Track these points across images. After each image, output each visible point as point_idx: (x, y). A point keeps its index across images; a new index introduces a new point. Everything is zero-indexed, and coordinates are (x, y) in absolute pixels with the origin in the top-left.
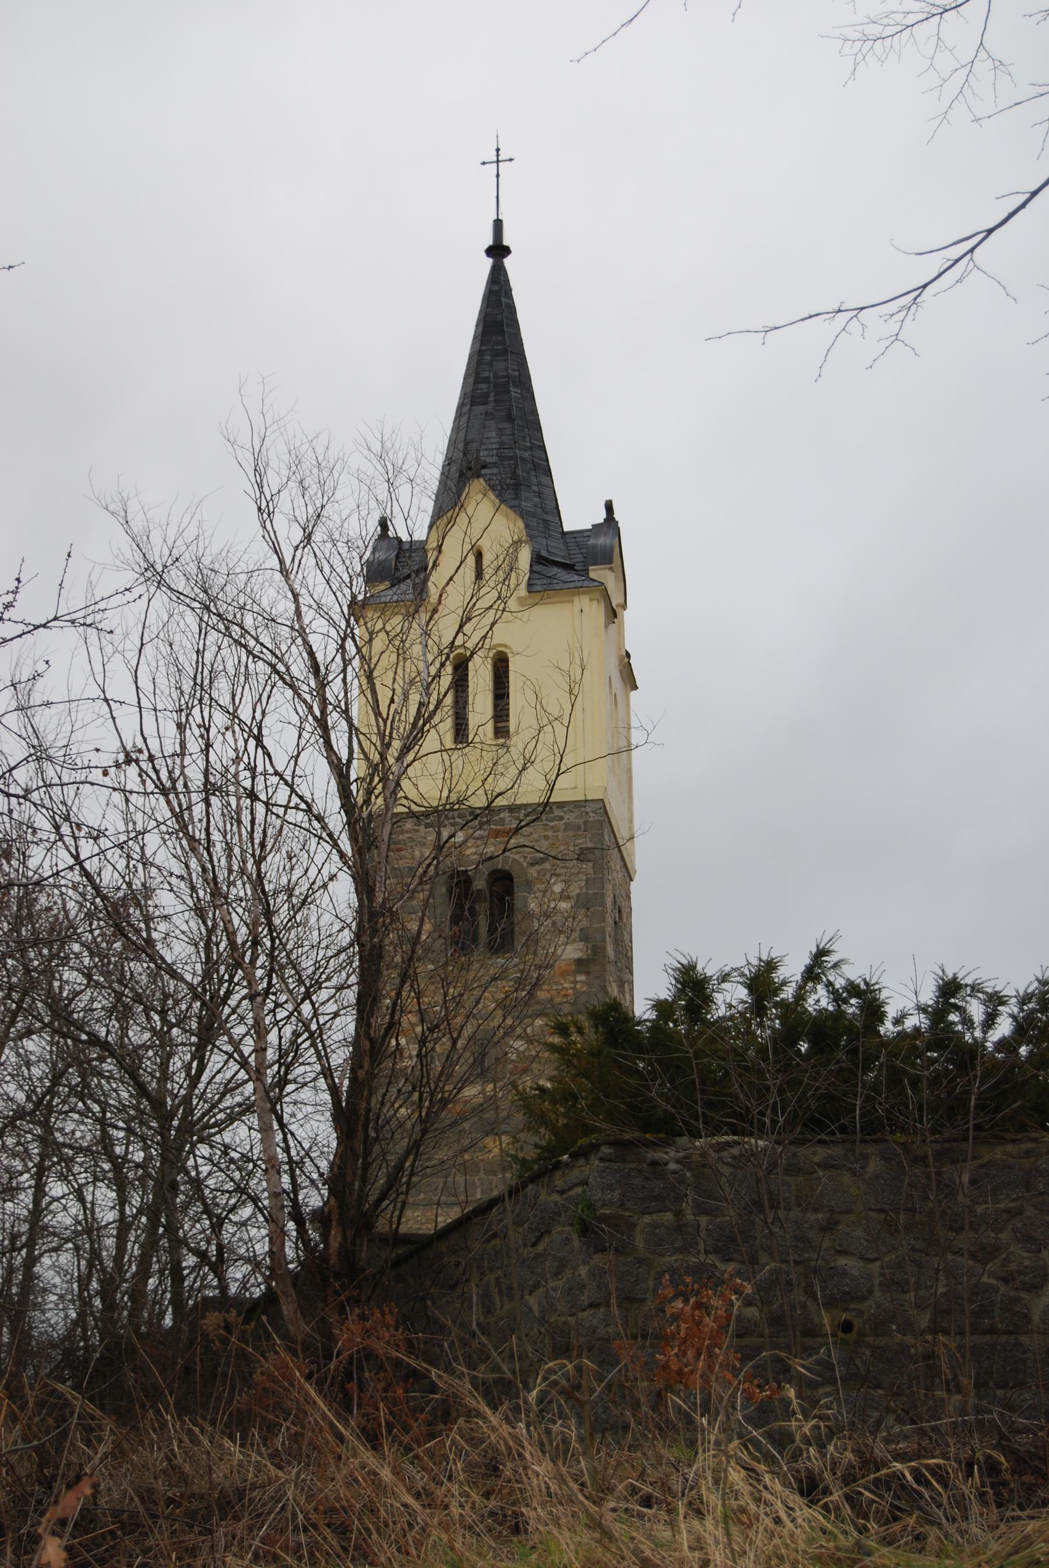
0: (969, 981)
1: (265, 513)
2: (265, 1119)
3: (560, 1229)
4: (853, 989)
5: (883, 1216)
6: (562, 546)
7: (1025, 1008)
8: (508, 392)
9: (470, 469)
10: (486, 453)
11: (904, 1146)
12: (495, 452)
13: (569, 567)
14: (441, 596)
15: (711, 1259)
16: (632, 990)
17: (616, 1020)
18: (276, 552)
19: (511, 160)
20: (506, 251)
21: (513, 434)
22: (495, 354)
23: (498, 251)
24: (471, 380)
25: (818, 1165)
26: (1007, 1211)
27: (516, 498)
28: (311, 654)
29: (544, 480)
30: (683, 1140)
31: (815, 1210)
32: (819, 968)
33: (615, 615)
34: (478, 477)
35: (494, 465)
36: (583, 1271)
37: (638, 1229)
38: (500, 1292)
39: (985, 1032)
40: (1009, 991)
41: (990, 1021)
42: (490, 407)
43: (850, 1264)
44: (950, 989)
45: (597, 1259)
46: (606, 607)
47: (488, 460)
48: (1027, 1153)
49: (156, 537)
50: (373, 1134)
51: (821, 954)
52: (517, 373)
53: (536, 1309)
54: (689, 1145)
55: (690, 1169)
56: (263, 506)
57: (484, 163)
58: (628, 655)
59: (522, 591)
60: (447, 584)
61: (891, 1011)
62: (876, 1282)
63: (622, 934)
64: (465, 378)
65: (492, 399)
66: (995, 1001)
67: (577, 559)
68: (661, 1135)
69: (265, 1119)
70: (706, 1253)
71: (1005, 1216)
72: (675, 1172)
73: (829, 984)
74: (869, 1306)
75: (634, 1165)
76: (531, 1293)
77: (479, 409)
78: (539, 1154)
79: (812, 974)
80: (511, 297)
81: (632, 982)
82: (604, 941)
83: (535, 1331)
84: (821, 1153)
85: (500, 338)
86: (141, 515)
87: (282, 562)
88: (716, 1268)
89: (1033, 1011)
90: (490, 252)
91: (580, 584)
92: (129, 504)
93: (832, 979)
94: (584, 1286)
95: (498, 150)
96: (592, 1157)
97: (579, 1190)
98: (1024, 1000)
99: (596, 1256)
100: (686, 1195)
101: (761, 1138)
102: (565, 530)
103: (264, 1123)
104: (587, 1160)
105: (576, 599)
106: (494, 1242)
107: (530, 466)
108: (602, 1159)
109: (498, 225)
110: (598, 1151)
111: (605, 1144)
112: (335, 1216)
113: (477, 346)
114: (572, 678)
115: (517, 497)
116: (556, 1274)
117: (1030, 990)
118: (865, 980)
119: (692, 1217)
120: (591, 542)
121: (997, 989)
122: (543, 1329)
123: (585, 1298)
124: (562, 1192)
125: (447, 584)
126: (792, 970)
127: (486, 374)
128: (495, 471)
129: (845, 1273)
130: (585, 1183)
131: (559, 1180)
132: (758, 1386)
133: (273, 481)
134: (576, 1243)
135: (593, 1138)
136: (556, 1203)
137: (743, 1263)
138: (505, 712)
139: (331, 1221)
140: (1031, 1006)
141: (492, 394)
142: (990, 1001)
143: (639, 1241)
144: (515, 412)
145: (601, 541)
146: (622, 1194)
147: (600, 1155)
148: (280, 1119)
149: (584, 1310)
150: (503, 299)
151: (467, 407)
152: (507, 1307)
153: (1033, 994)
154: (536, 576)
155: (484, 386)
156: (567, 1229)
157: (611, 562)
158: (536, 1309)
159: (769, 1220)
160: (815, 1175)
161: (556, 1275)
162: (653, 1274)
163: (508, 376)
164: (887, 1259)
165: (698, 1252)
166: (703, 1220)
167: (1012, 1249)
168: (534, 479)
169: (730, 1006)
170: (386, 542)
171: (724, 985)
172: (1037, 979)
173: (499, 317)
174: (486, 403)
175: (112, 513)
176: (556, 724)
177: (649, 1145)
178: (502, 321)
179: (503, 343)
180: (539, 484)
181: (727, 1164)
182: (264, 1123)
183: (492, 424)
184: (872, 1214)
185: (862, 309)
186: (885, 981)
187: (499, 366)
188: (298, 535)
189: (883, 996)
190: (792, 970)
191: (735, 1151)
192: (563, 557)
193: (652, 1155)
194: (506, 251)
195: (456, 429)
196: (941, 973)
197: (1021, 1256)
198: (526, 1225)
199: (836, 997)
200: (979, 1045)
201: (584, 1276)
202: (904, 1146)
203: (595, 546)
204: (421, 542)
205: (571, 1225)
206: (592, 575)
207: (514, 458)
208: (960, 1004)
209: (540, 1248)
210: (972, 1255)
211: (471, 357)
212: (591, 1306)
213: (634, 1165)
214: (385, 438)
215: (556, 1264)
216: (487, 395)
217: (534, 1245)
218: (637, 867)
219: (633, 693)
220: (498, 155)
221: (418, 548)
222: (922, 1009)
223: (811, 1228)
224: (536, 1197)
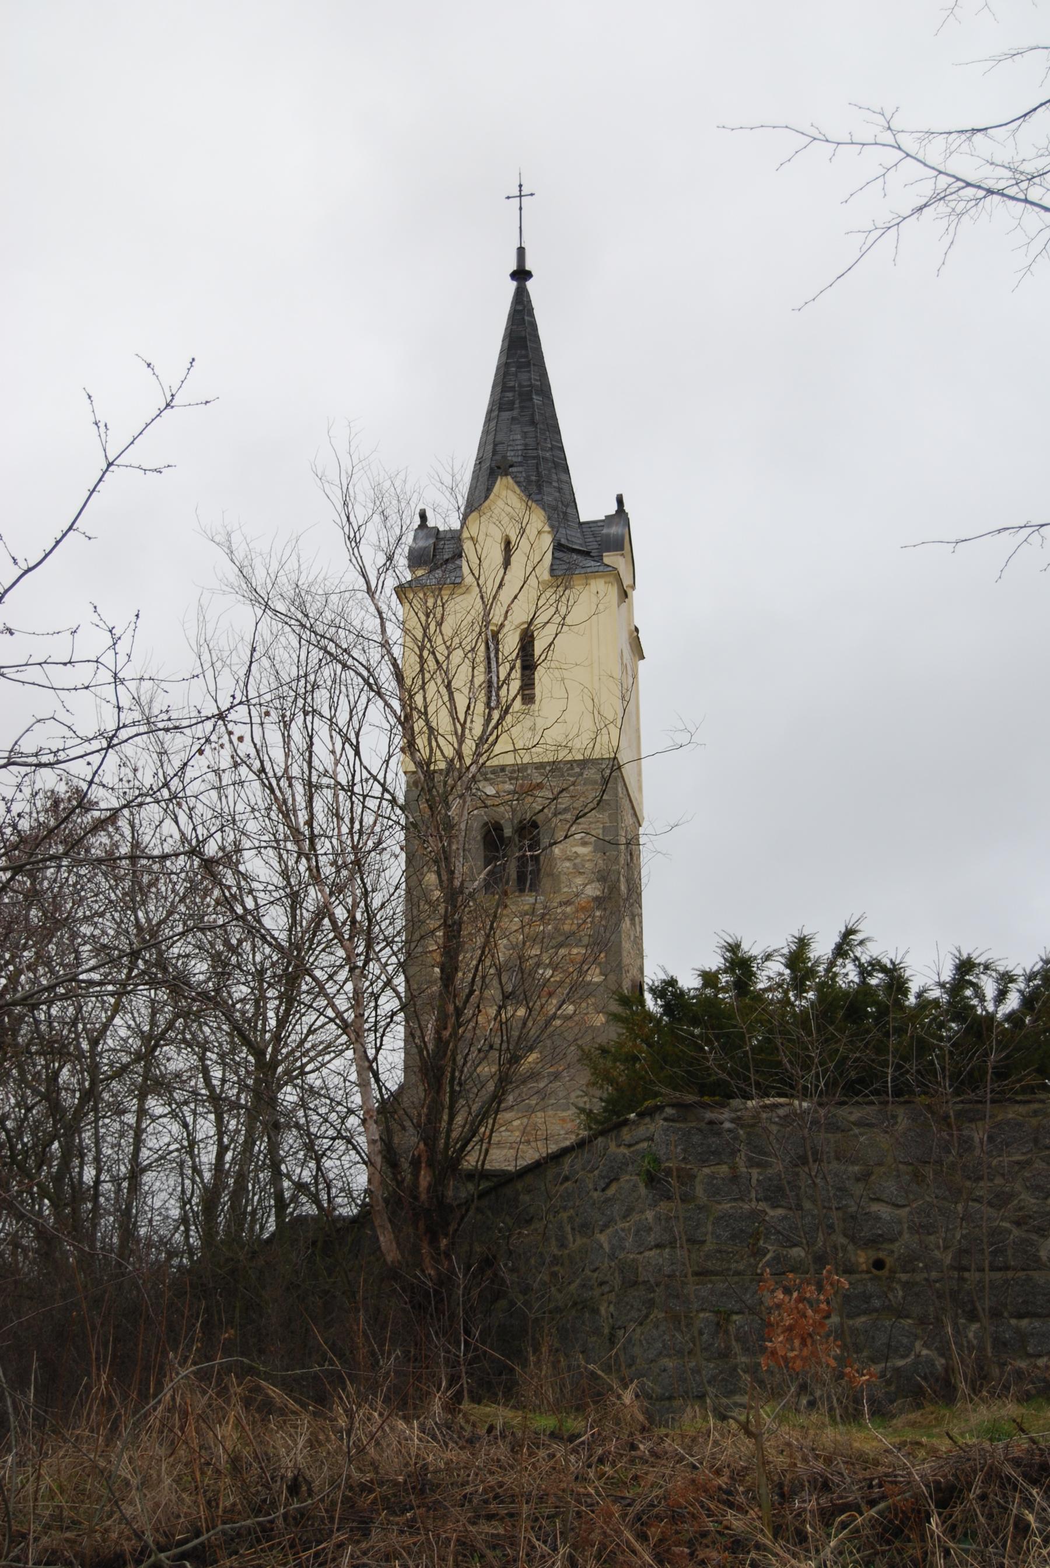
0: (981, 960)
1: (354, 541)
2: (364, 1076)
3: (627, 1178)
4: (877, 965)
5: (910, 1168)
6: (579, 535)
7: (1031, 984)
8: (531, 399)
9: (499, 468)
10: (512, 453)
11: (929, 1107)
12: (520, 453)
13: (587, 554)
14: (507, 612)
15: (762, 1206)
16: (641, 922)
17: (673, 994)
18: (364, 576)
19: (532, 195)
20: (528, 275)
21: (536, 437)
22: (520, 366)
23: (521, 275)
24: (499, 389)
25: (854, 1124)
26: (1018, 1163)
27: (540, 493)
28: (395, 664)
29: (563, 477)
30: (736, 1102)
31: (853, 1163)
32: (848, 945)
33: (626, 596)
34: (506, 475)
35: (520, 464)
36: (650, 1215)
37: (698, 1180)
38: (573, 1229)
39: (997, 1006)
40: (1018, 971)
41: (1001, 996)
42: (515, 413)
43: (884, 1211)
44: (965, 966)
45: (663, 1206)
46: (618, 588)
47: (515, 459)
48: (1035, 1113)
49: (258, 563)
50: (458, 1089)
51: (849, 932)
52: (538, 383)
53: (606, 1246)
54: (742, 1107)
55: (742, 1126)
56: (352, 536)
57: (508, 198)
58: (637, 630)
59: (546, 576)
60: (513, 602)
61: (914, 987)
62: (905, 1226)
63: (633, 874)
64: (493, 387)
65: (517, 406)
66: (1006, 979)
67: (593, 546)
68: (717, 1098)
69: (364, 1076)
70: (758, 1200)
71: (1016, 1168)
72: (730, 1130)
73: (856, 959)
74: (898, 1248)
75: (693, 1124)
76: (601, 1231)
77: (506, 415)
78: (604, 1108)
79: (841, 951)
80: (532, 315)
81: (641, 915)
82: (619, 880)
83: (606, 1265)
84: (856, 1114)
85: (523, 352)
86: (244, 545)
87: (368, 583)
88: (766, 1214)
89: (1037, 987)
90: (514, 275)
91: (596, 569)
92: (232, 536)
93: (858, 954)
94: (651, 1229)
95: (520, 186)
96: (657, 1117)
97: (645, 1145)
98: (1030, 977)
99: (662, 1203)
100: (739, 1151)
101: (804, 1101)
102: (582, 520)
103: (363, 1080)
104: (653, 1120)
105: (593, 582)
106: (566, 1184)
107: (550, 464)
108: (665, 1119)
109: (521, 252)
110: (662, 1112)
111: (669, 1105)
112: (424, 1159)
113: (504, 359)
114: (625, 686)
115: (540, 491)
116: (625, 1217)
117: (1035, 969)
118: (891, 961)
119: (744, 1170)
120: (605, 531)
121: (1008, 969)
122: (613, 1264)
123: (651, 1239)
124: (630, 1146)
125: (513, 602)
126: (822, 949)
127: (512, 384)
128: (520, 469)
129: (878, 1218)
130: (651, 1139)
131: (626, 1135)
132: (857, 1371)
133: (359, 514)
134: (643, 1190)
135: (658, 1101)
136: (624, 1155)
137: (791, 1209)
138: (530, 682)
139: (420, 1163)
140: (1036, 982)
141: (517, 402)
142: (1001, 979)
143: (699, 1191)
144: (537, 417)
145: (614, 530)
146: (684, 1150)
147: (664, 1115)
148: (376, 1075)
149: (651, 1249)
150: (526, 318)
151: (496, 413)
152: (579, 1242)
153: (1038, 972)
154: (558, 562)
155: (510, 394)
156: (634, 1178)
157: (622, 549)
158: (606, 1246)
159: (813, 1174)
160: (852, 1133)
161: (624, 1217)
162: (711, 1219)
163: (530, 386)
164: (914, 1206)
165: (751, 1200)
166: (755, 1172)
167: (1022, 1197)
168: (554, 477)
169: (769, 978)
170: (425, 531)
171: (768, 964)
172: (1042, 960)
173: (523, 334)
174: (512, 410)
175: (218, 544)
176: (611, 727)
177: (705, 1106)
178: (525, 337)
179: (526, 356)
180: (559, 480)
181: (775, 1123)
182: (363, 1080)
183: (516, 427)
184: (901, 1166)
185: (1042, 526)
186: (908, 961)
187: (523, 376)
188: (381, 559)
189: (907, 974)
190: (822, 949)
191: (781, 1112)
192: (581, 545)
193: (709, 1115)
194: (528, 275)
195: (486, 432)
196: (958, 955)
197: (1029, 1200)
198: (596, 1172)
199: (864, 972)
200: (991, 1017)
201: (650, 1220)
202: (929, 1107)
203: (608, 535)
204: (456, 531)
205: (638, 1175)
206: (606, 560)
207: (537, 457)
208: (975, 980)
209: (611, 1191)
210: (990, 1204)
211: (498, 369)
212: (658, 1246)
213: (693, 1124)
214: (456, 471)
215: (624, 1208)
216: (513, 403)
217: (603, 1190)
218: (645, 815)
219: (641, 662)
220: (520, 191)
221: (455, 537)
222: (942, 985)
223: (848, 1178)
224: (606, 1148)
